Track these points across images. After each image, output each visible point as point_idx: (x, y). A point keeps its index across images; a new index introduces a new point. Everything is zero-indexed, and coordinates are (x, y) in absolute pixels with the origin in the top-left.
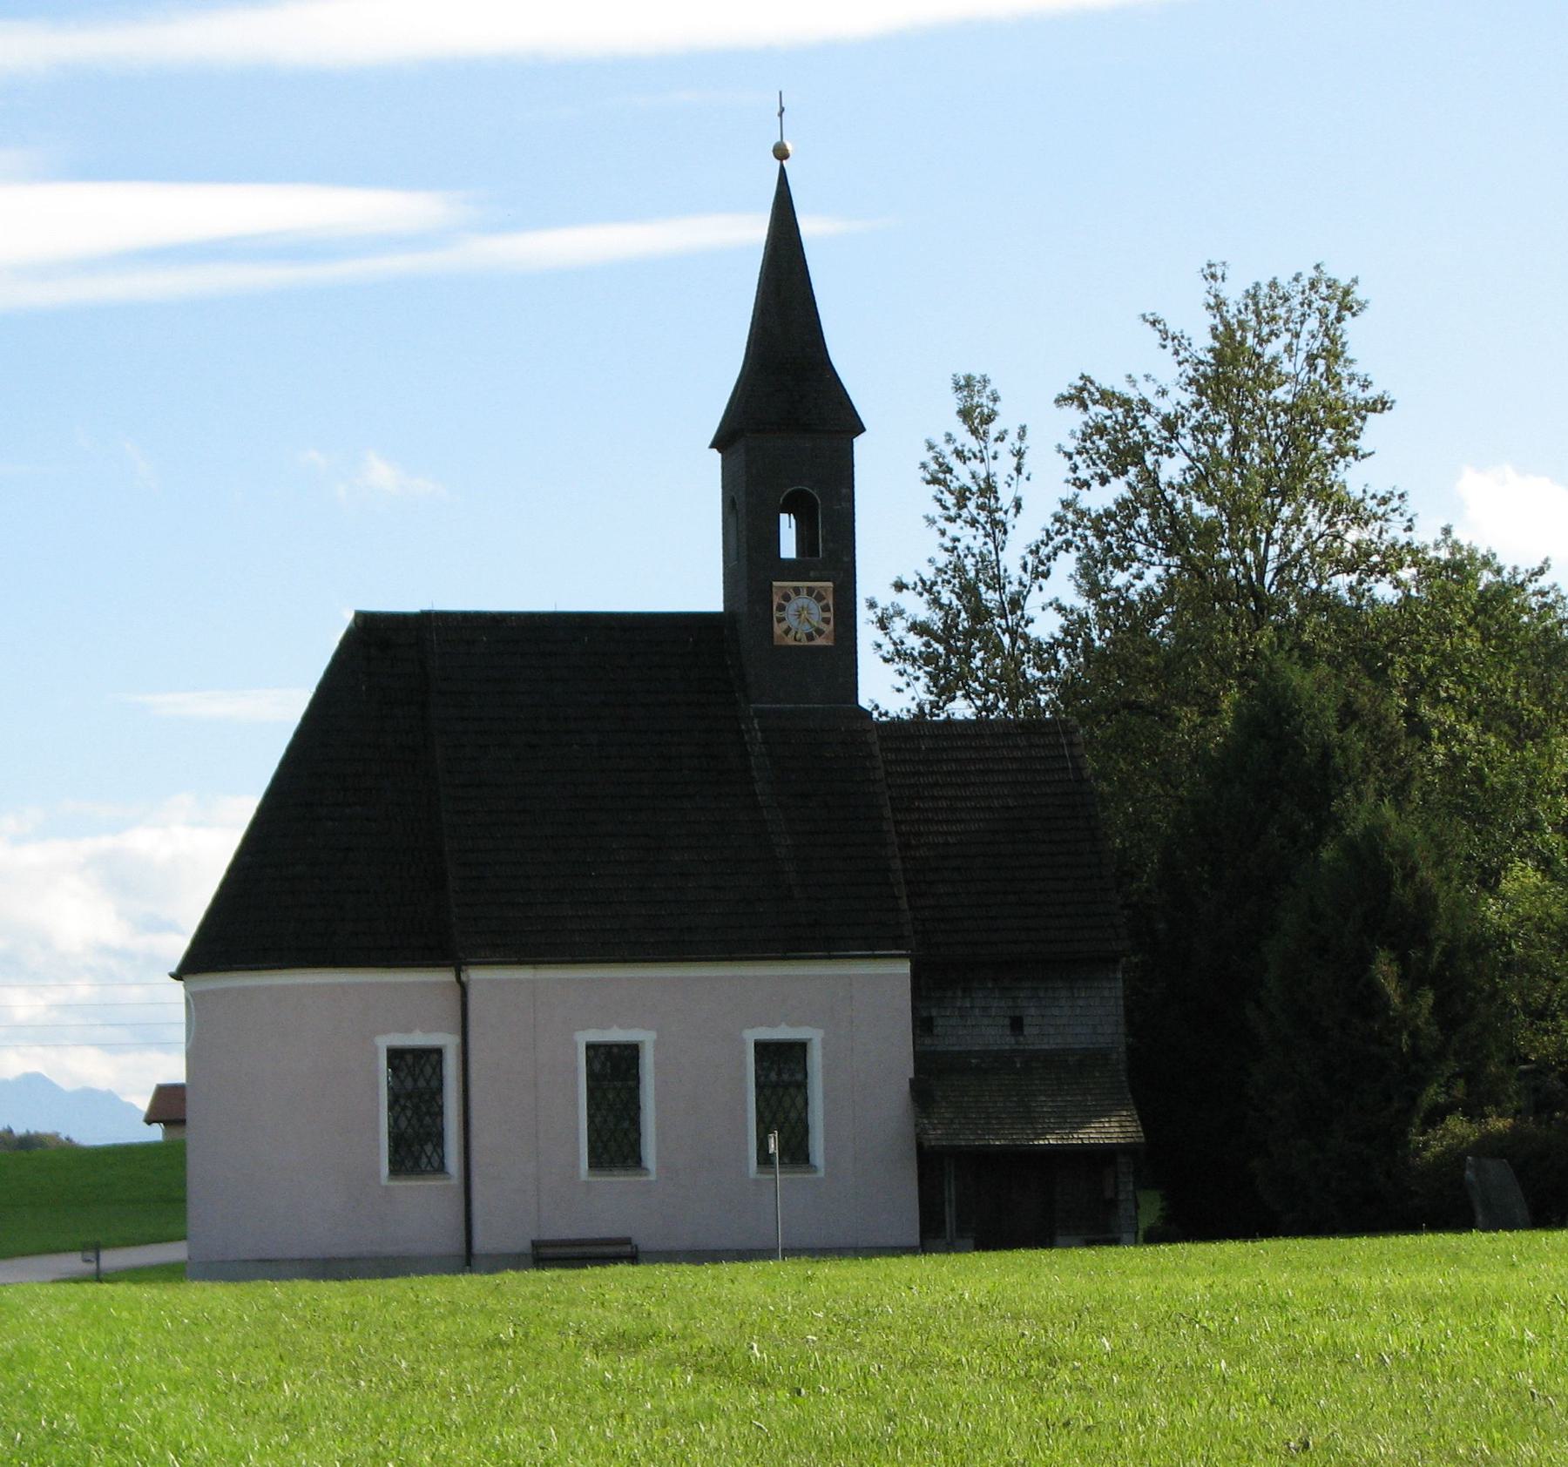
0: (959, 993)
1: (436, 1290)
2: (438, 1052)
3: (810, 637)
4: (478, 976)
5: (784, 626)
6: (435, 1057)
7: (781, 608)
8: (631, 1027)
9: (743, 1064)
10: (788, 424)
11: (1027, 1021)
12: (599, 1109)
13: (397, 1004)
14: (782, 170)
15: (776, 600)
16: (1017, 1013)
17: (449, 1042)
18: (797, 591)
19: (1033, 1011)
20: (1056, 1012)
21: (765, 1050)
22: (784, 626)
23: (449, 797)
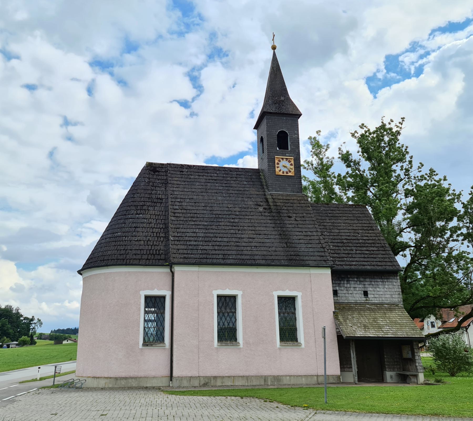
0: (346, 282)
1: (161, 398)
2: (164, 297)
3: (287, 173)
4: (178, 269)
5: (279, 169)
6: (232, 299)
7: (278, 164)
8: (233, 289)
9: (273, 304)
10: (278, 119)
11: (369, 292)
12: (221, 319)
13: (153, 280)
14: (274, 54)
15: (276, 161)
16: (366, 290)
17: (168, 294)
18: (282, 159)
19: (371, 289)
20: (378, 289)
21: (281, 299)
22: (279, 169)
23: (162, 219)
